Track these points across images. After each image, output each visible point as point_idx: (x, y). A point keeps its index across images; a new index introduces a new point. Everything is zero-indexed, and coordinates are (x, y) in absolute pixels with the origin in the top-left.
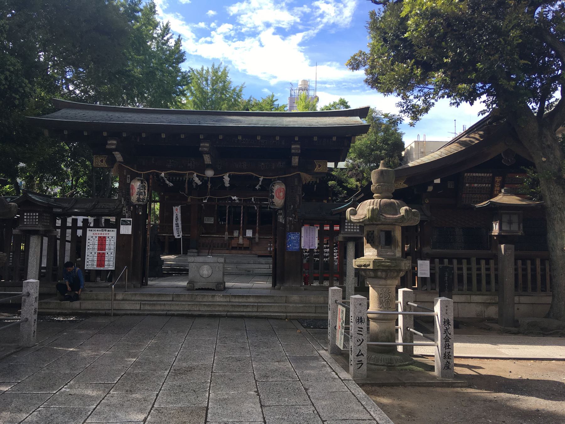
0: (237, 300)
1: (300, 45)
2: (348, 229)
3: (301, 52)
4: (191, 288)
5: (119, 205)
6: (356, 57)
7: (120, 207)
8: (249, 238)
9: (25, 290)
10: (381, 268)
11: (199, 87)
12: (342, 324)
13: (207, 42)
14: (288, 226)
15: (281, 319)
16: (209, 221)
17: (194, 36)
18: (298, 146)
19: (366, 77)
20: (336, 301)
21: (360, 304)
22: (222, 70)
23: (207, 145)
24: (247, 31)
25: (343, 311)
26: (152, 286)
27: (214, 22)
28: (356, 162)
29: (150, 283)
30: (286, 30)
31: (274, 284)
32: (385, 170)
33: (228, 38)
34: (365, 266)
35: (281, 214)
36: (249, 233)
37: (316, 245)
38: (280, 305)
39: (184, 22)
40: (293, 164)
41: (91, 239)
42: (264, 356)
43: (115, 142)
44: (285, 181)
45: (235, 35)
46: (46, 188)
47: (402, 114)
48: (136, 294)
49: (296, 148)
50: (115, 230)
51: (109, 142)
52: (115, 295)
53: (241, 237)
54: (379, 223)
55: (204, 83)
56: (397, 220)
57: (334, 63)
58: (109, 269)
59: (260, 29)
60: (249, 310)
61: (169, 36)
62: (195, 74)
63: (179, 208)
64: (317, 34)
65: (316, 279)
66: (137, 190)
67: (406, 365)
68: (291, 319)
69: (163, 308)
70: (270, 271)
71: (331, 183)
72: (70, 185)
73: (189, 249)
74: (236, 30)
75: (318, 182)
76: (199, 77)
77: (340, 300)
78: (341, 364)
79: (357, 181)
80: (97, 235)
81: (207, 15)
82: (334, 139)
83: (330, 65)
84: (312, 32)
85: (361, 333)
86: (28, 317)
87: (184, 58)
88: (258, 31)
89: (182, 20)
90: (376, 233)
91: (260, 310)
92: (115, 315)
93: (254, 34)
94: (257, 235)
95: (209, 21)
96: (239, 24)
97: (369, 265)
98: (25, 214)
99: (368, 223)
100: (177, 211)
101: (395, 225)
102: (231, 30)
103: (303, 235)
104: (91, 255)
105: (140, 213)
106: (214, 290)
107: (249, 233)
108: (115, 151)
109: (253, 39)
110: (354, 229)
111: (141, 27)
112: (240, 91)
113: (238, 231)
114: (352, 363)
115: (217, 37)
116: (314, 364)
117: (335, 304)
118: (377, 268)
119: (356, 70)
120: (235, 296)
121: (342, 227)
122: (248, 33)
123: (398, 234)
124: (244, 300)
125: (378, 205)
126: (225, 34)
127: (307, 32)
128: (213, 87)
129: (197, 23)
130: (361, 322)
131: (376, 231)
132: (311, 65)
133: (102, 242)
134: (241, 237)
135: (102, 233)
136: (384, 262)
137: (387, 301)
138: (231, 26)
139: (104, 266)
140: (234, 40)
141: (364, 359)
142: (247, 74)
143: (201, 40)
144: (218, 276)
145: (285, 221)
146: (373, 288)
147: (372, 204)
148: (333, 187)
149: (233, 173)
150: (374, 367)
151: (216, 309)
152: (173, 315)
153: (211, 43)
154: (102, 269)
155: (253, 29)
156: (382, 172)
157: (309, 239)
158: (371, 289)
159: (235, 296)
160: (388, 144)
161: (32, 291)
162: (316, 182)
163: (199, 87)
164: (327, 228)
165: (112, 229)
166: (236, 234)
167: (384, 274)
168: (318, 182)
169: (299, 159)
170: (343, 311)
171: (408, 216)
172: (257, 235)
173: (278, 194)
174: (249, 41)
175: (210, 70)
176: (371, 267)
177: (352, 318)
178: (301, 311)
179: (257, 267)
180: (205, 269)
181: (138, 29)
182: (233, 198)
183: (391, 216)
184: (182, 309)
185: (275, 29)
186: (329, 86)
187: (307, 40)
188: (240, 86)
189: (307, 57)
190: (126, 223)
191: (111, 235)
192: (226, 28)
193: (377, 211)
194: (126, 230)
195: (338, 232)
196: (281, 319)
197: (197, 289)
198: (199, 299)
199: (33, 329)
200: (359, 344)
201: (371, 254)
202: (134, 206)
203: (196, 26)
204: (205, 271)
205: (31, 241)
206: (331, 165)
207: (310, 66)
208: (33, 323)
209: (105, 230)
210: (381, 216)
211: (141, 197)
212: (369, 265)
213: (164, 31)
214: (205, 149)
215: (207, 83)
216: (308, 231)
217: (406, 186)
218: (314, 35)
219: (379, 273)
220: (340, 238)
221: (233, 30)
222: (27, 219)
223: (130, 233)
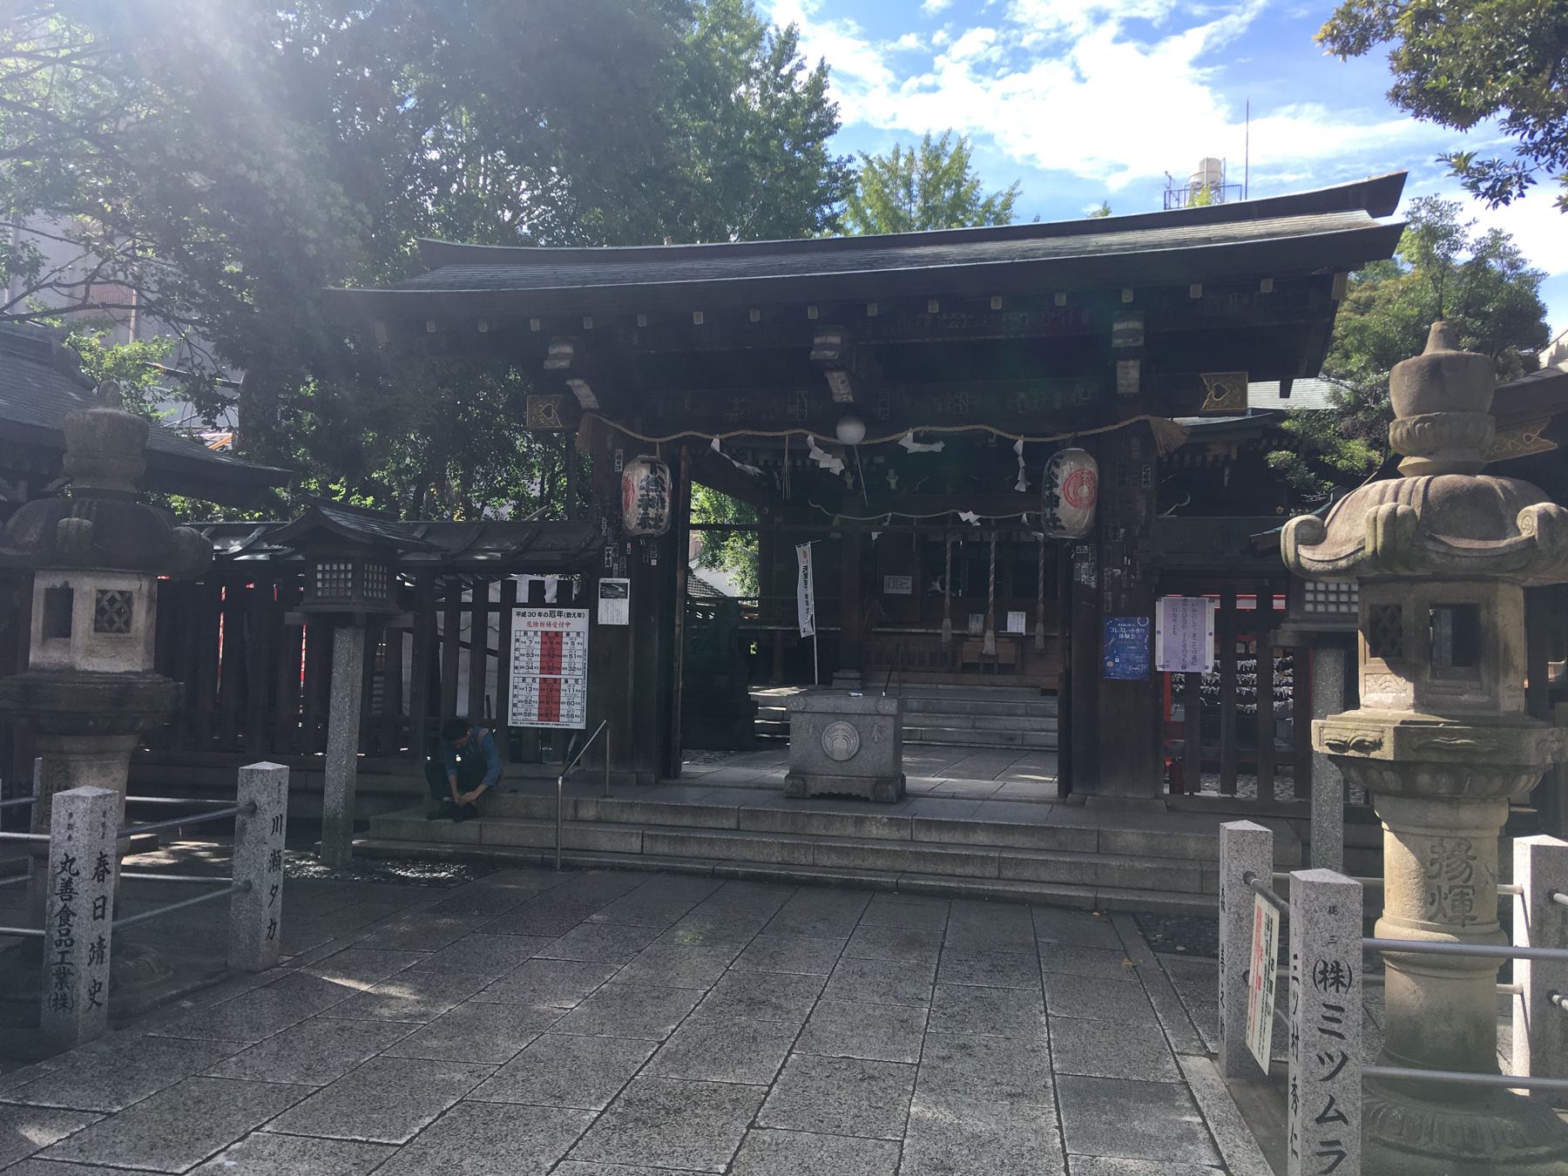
0: (934, 836)
1: (1199, 62)
2: (1315, 603)
3: (1202, 83)
4: (798, 791)
5: (593, 539)
6: (1355, 10)
7: (597, 544)
8: (1015, 637)
9: (243, 796)
10: (1433, 757)
11: (886, 205)
12: (1267, 973)
13: (923, 89)
14: (1109, 596)
15: (1079, 909)
16: (900, 586)
17: (890, 77)
18: (1137, 325)
19: (1391, 81)
20: (1247, 876)
21: (1333, 910)
22: (951, 149)
23: (835, 340)
24: (1037, 43)
25: (1270, 921)
26: (693, 781)
27: (942, 27)
28: (1367, 383)
29: (687, 767)
30: (1155, 24)
31: (1065, 787)
32: (1448, 358)
33: (982, 68)
34: (1360, 745)
35: (1083, 558)
36: (1016, 623)
37: (1207, 662)
38: (1076, 859)
39: (866, 43)
40: (1121, 390)
41: (523, 639)
42: (968, 1066)
43: (568, 350)
44: (1095, 448)
45: (1002, 57)
46: (479, 506)
47: (1528, 160)
48: (632, 806)
49: (1125, 330)
50: (586, 612)
51: (553, 351)
52: (576, 805)
53: (990, 634)
54: (1420, 572)
55: (902, 192)
56: (1504, 555)
57: (1308, 107)
58: (572, 726)
59: (1073, 31)
60: (969, 870)
61: (794, 62)
62: (875, 172)
64: (1252, 25)
65: (1210, 768)
66: (638, 493)
67: (1540, 1159)
68: (1111, 913)
69: (705, 850)
70: (1053, 738)
71: (1278, 457)
72: (536, 493)
74: (1006, 43)
75: (1234, 456)
76: (886, 177)
77: (1266, 875)
78: (1262, 1131)
79: (1371, 447)
80: (539, 628)
81: (924, 11)
82: (1267, 286)
83: (1294, 115)
84: (1236, 22)
85: (1335, 1026)
86: (252, 877)
87: (836, 120)
88: (1068, 39)
89: (860, 37)
90: (1409, 615)
91: (1009, 874)
92: (568, 866)
93: (1057, 48)
94: (1040, 627)
95: (927, 26)
96: (1013, 25)
97: (1378, 745)
98: (320, 567)
99: (1373, 574)
100: (804, 556)
101: (1496, 580)
102: (991, 46)
103: (1160, 626)
104: (523, 685)
105: (654, 563)
106: (866, 799)
107: (1016, 623)
108: (572, 378)
109: (1054, 62)
110: (1326, 603)
111: (706, 38)
112: (1007, 205)
113: (981, 617)
114: (1297, 1145)
115: (952, 69)
116: (1147, 1123)
117: (1245, 890)
118: (1413, 757)
119: (1357, 53)
120: (929, 825)
121: (1295, 598)
122: (1040, 48)
123: (1509, 617)
124: (958, 837)
125: (1417, 501)
126: (973, 58)
127: (1218, 23)
128: (926, 202)
129: (896, 39)
130: (1337, 981)
131: (1403, 601)
132: (1233, 121)
133: (552, 645)
135: (552, 620)
136: (1442, 732)
137: (1462, 893)
138: (989, 34)
139: (557, 717)
140: (1002, 71)
141: (1349, 1135)
142: (1039, 166)
143: (906, 86)
144: (878, 757)
145: (1100, 581)
146: (1400, 835)
147: (1389, 494)
148: (1282, 471)
149: (928, 429)
150: (1398, 1158)
151: (867, 864)
152: (732, 877)
153: (934, 89)
154: (551, 725)
155: (1054, 35)
156: (1436, 365)
157: (1184, 638)
158: (1389, 839)
159: (929, 825)
160: (1486, 315)
161: (262, 800)
162: (1228, 456)
163: (886, 205)
164: (1246, 604)
165: (577, 611)
166: (975, 626)
167: (1444, 785)
168: (1234, 456)
169: (1144, 372)
170: (1270, 921)
171: (1552, 541)
172: (1040, 627)
173: (1074, 488)
174: (1043, 71)
175: (918, 154)
176: (1387, 752)
177: (1298, 963)
178: (1148, 884)
179: (1035, 726)
180: (840, 734)
181: (700, 44)
182: (964, 516)
183: (1477, 544)
184: (761, 858)
185: (1122, 24)
186: (1294, 177)
187: (1218, 46)
188: (1006, 190)
189: (1222, 96)
190: (612, 592)
191: (575, 625)
192: (977, 41)
193: (1409, 525)
194: (615, 612)
195: (1281, 616)
196: (1079, 909)
197: (814, 797)
198: (817, 828)
199: (266, 914)
200: (1326, 1070)
201: (1388, 698)
202: (635, 540)
203: (891, 46)
204: (840, 740)
205: (338, 645)
206: (1263, 395)
207: (1230, 122)
208: (265, 897)
209: (560, 614)
210: (1430, 545)
211: (652, 512)
212: (1378, 745)
213: (782, 52)
214: (829, 354)
215: (910, 194)
216: (1180, 614)
217: (1551, 445)
218: (1242, 30)
219: (1424, 780)
220: (1286, 635)
221: (996, 43)
222: (323, 580)
223: (625, 621)
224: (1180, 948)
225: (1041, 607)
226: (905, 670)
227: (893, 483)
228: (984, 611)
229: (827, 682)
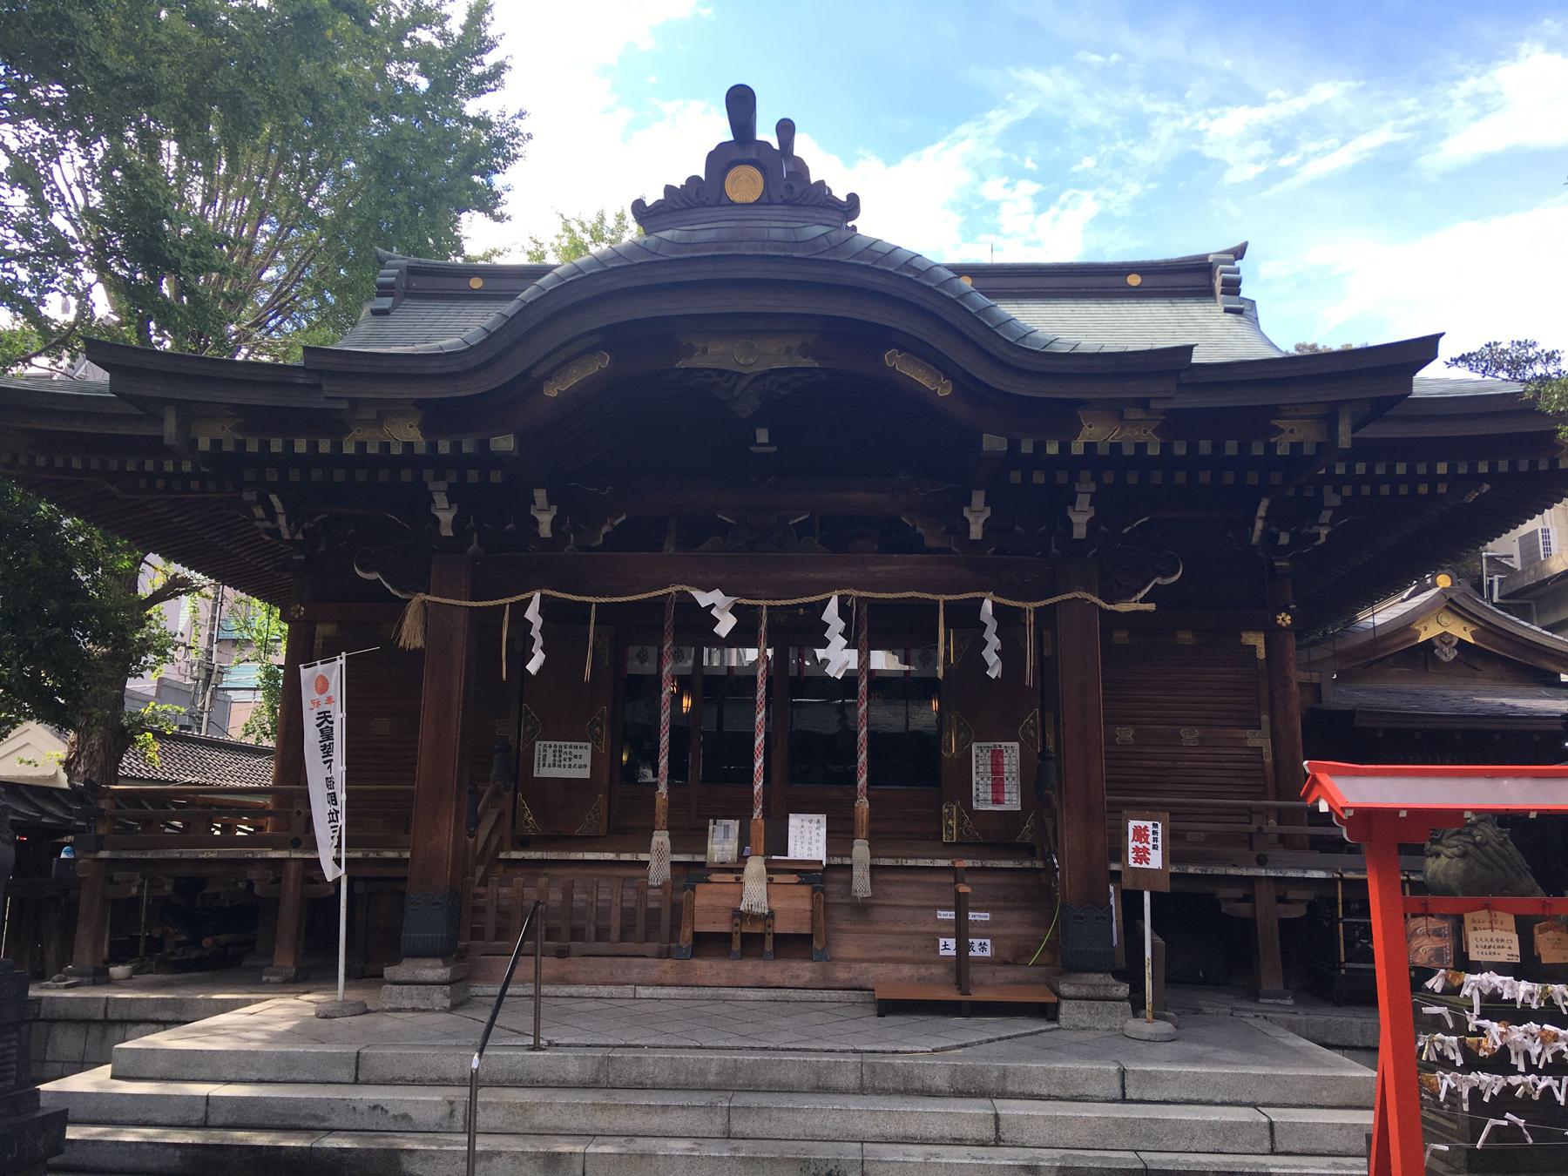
8: (806, 872)
16: (566, 762)
36: (807, 838)
53: (755, 866)
63: (973, 536)
73: (396, 960)
94: (861, 851)
107: (807, 838)
113: (734, 825)
134: (755, 866)
166: (722, 843)
172: (861, 851)
224: (686, 702)
225: (863, 804)
226: (562, 954)
227: (545, 521)
228: (741, 811)
229: (365, 972)
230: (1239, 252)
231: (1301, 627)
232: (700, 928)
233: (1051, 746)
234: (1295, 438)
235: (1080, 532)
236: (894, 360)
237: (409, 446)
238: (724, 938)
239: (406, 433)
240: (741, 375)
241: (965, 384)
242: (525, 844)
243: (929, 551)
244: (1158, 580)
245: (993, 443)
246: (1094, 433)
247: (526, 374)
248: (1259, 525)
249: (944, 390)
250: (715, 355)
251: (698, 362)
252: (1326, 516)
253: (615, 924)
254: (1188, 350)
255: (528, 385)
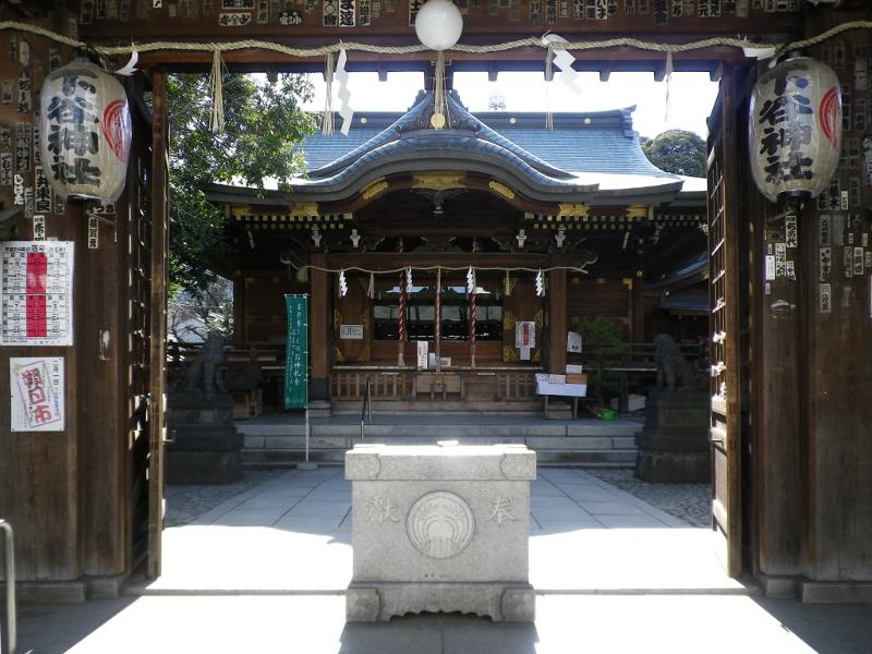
230: (633, 109)
231: (649, 278)
232: (420, 390)
233: (547, 324)
234: (635, 215)
235: (560, 244)
236: (492, 185)
237: (314, 218)
238: (429, 394)
239: (312, 212)
240: (436, 191)
241: (518, 194)
242: (339, 364)
243: (502, 251)
244: (588, 262)
245: (529, 216)
246: (565, 211)
247: (357, 192)
248: (626, 242)
249: (511, 196)
250: (427, 182)
251: (420, 186)
252: (657, 233)
253: (376, 391)
254: (597, 185)
255: (358, 195)
